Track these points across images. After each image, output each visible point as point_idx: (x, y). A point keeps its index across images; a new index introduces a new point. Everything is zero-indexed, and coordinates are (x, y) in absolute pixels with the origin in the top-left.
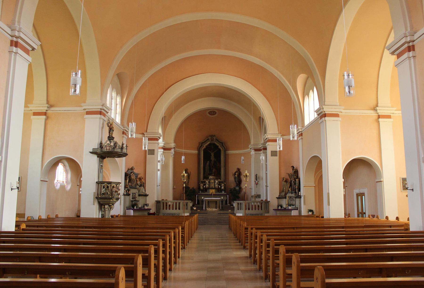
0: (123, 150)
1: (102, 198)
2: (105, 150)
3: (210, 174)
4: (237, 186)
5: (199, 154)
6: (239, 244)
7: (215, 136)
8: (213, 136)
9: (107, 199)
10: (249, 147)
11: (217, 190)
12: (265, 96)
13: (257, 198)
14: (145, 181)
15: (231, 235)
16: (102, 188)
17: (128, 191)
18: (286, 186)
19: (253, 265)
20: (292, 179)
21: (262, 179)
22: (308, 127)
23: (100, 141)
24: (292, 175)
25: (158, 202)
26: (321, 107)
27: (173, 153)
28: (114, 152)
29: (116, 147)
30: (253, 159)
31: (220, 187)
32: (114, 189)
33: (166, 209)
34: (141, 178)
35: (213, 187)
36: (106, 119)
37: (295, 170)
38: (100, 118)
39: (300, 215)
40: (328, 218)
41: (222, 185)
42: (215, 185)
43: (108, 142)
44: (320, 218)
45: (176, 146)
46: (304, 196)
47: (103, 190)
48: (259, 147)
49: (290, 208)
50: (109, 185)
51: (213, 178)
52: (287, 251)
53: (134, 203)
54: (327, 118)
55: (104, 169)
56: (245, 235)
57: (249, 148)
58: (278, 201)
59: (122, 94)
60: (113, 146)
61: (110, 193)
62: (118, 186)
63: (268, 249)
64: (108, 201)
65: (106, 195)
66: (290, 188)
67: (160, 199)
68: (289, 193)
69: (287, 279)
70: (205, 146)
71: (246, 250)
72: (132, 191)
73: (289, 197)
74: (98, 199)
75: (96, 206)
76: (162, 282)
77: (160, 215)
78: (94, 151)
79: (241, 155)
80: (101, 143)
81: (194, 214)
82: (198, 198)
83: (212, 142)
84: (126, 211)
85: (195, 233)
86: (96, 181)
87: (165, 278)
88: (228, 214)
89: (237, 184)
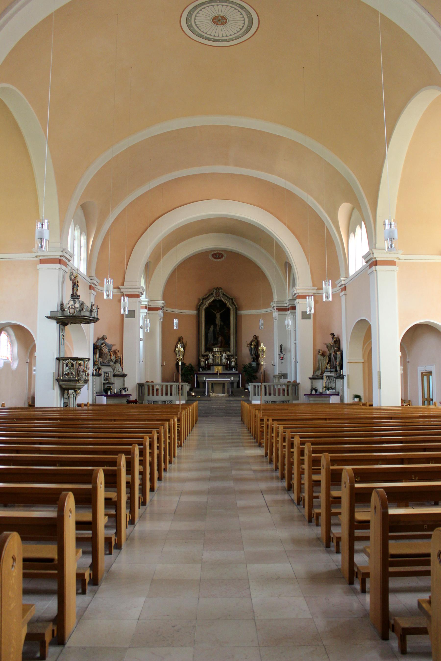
0: (93, 313)
1: (64, 380)
2: (67, 313)
3: (215, 345)
4: (254, 361)
5: (198, 316)
6: (253, 441)
7: (221, 289)
8: (219, 290)
9: (72, 381)
10: (271, 304)
11: (225, 367)
12: (294, 233)
13: (281, 378)
15: (244, 430)
16: (65, 365)
17: (98, 370)
18: (323, 361)
19: (269, 465)
20: (331, 352)
22: (358, 275)
23: (60, 301)
24: (332, 346)
25: (141, 385)
26: (371, 252)
27: (162, 315)
28: (80, 316)
29: (83, 309)
30: (276, 324)
32: (82, 368)
33: (153, 395)
34: (116, 351)
36: (67, 269)
37: (336, 339)
38: (60, 269)
39: (342, 403)
40: (379, 406)
41: (233, 360)
42: (221, 360)
43: (72, 303)
44: (367, 406)
45: (165, 304)
46: (348, 375)
47: (66, 370)
48: (285, 306)
49: (328, 392)
50: (74, 363)
51: (219, 350)
52: (334, 461)
53: (107, 386)
54: (378, 267)
55: (66, 342)
56: (261, 428)
57: (271, 307)
58: (312, 383)
59: (87, 232)
60: (79, 308)
61: (76, 374)
62: (87, 364)
63: (301, 458)
64: (74, 384)
65: (70, 377)
66: (329, 364)
67: (143, 381)
69: (391, 569)
70: (207, 304)
71: (262, 448)
72: (104, 370)
74: (59, 382)
75: (57, 391)
76: (139, 508)
77: (143, 403)
78: (52, 316)
79: (258, 316)
80: (62, 305)
81: (192, 402)
82: (198, 379)
84: (95, 398)
85: (194, 427)
86: (56, 357)
87: (160, 479)
88: (240, 401)
89: (254, 359)
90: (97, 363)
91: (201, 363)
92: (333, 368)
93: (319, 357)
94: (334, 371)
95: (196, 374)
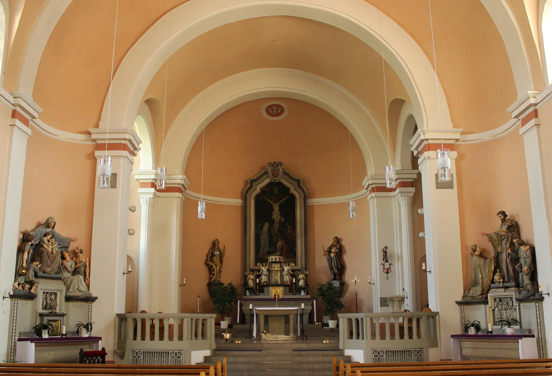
4: (335, 279)
5: (245, 207)
7: (281, 164)
8: (277, 165)
11: (288, 288)
12: (412, 35)
14: (88, 259)
21: (398, 259)
31: (294, 281)
35: (279, 283)
41: (301, 276)
42: (282, 277)
49: (509, 331)
51: (278, 261)
58: (462, 312)
63: (337, 373)
66: (498, 274)
68: (493, 288)
73: (495, 299)
82: (243, 308)
83: (274, 180)
84: (15, 346)
89: (335, 274)
90: (24, 271)
91: (248, 282)
92: (509, 281)
93: (476, 259)
94: (512, 287)
95: (239, 299)
